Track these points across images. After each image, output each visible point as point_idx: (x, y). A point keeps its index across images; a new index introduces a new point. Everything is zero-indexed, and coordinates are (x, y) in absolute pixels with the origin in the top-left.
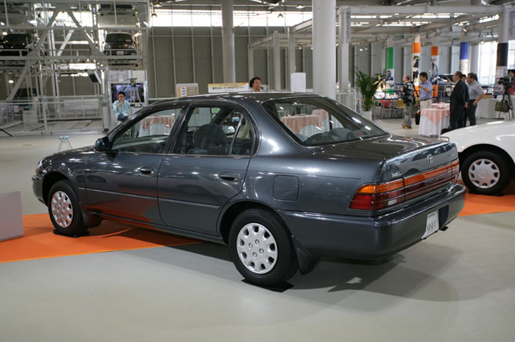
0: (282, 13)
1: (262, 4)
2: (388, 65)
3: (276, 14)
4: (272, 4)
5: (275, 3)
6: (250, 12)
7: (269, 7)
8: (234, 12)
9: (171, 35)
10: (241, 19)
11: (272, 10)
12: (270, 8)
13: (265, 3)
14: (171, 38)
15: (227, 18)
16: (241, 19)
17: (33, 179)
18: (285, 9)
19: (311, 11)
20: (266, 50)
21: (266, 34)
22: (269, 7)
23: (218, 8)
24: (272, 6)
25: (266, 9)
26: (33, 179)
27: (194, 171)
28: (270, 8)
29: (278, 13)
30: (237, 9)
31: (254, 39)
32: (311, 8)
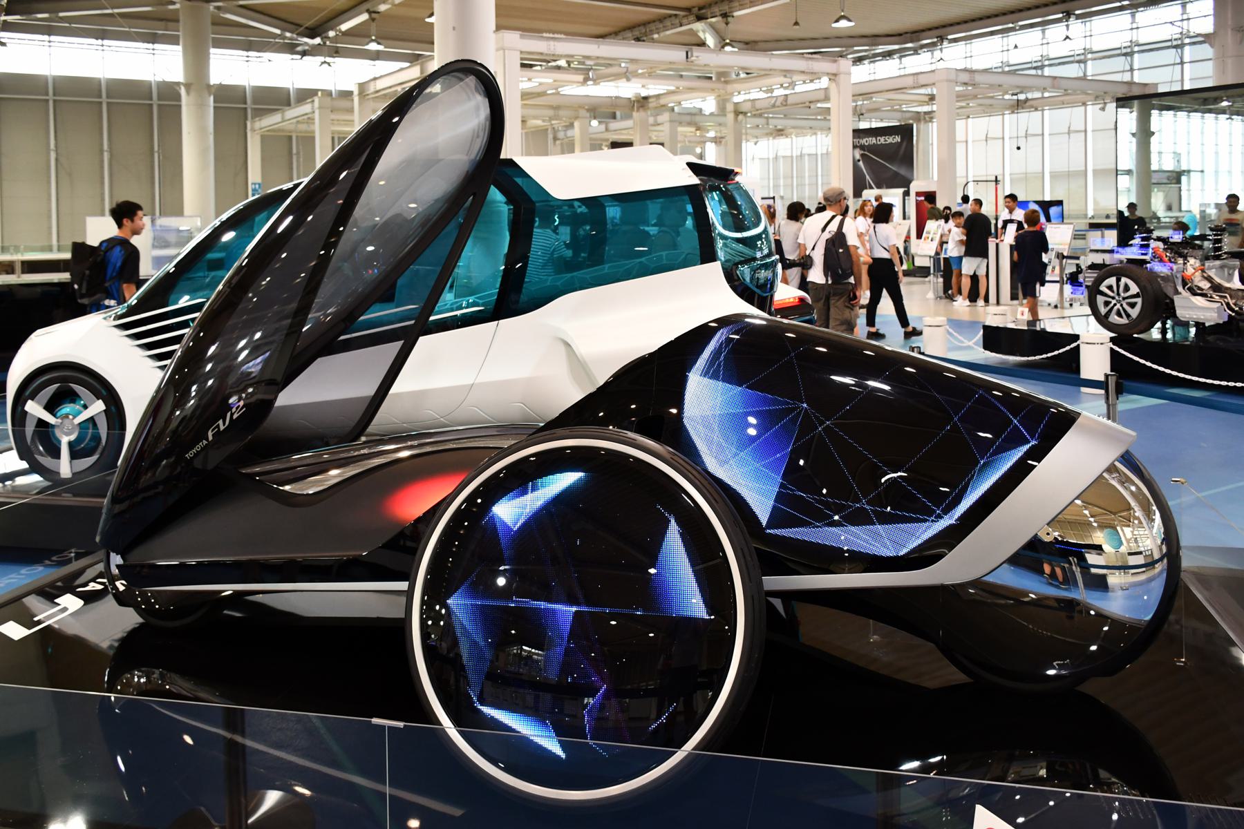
0: (328, 59)
1: (281, 36)
2: (871, 141)
3: (313, 61)
4: (306, 40)
5: (313, 37)
6: (251, 53)
7: (298, 45)
8: (212, 50)
9: (100, 96)
10: (232, 68)
11: (304, 54)
12: (299, 49)
13: (288, 34)
14: (47, 101)
15: (197, 63)
16: (232, 68)
17: (1133, 135)
18: (336, 52)
19: (178, 44)
20: (290, 138)
21: (289, 104)
22: (298, 45)
23: (174, 41)
24: (306, 44)
25: (291, 48)
26: (1133, 135)
27: (208, 348)
28: (299, 49)
29: (322, 59)
30: (219, 44)
31: (260, 113)
32: (178, 36)
